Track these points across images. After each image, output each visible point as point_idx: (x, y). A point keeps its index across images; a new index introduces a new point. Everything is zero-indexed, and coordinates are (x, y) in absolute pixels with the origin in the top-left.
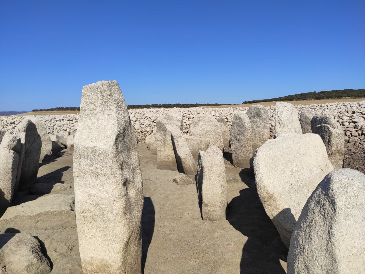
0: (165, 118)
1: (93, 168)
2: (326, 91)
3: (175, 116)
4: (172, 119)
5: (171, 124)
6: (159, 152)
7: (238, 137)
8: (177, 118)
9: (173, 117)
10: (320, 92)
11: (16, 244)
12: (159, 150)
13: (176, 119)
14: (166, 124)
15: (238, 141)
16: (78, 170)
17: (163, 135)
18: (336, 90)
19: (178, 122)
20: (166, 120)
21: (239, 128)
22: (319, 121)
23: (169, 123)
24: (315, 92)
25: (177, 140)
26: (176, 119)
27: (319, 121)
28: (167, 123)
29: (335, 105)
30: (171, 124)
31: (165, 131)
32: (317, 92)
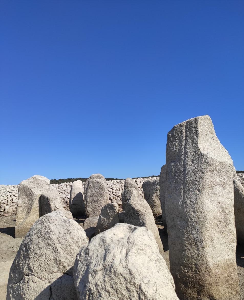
0: (31, 182)
1: (222, 180)
2: (63, 179)
3: (43, 180)
4: (40, 182)
5: (38, 188)
6: (18, 219)
7: (95, 199)
8: (45, 181)
9: (41, 181)
10: (59, 180)
11: (96, 272)
12: (19, 217)
13: (44, 182)
14: (32, 188)
15: (96, 202)
16: (210, 182)
17: (27, 200)
18: (71, 178)
19: (46, 186)
20: (32, 184)
21: (97, 191)
22: (152, 183)
23: (36, 187)
24: (55, 180)
25: (54, 202)
26: (44, 182)
27: (152, 183)
28: (34, 187)
29: (112, 182)
30: (38, 188)
31: (31, 195)
32: (56, 180)
